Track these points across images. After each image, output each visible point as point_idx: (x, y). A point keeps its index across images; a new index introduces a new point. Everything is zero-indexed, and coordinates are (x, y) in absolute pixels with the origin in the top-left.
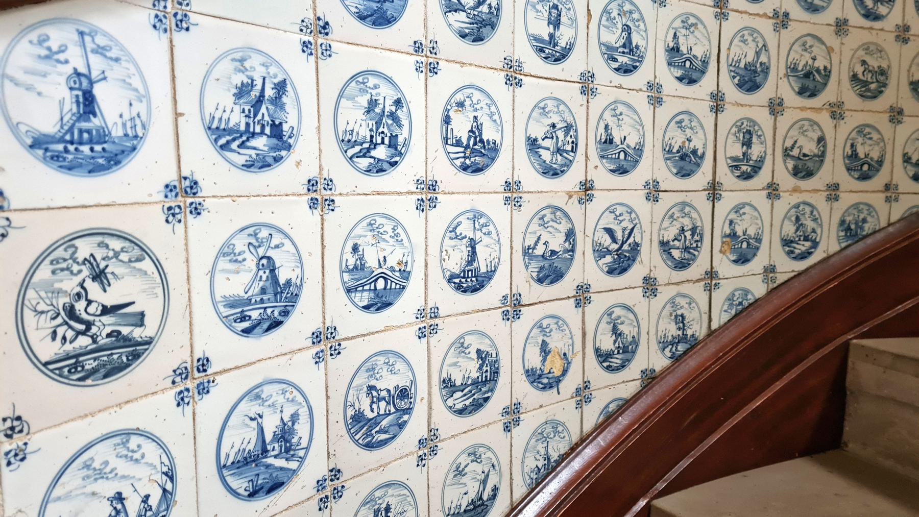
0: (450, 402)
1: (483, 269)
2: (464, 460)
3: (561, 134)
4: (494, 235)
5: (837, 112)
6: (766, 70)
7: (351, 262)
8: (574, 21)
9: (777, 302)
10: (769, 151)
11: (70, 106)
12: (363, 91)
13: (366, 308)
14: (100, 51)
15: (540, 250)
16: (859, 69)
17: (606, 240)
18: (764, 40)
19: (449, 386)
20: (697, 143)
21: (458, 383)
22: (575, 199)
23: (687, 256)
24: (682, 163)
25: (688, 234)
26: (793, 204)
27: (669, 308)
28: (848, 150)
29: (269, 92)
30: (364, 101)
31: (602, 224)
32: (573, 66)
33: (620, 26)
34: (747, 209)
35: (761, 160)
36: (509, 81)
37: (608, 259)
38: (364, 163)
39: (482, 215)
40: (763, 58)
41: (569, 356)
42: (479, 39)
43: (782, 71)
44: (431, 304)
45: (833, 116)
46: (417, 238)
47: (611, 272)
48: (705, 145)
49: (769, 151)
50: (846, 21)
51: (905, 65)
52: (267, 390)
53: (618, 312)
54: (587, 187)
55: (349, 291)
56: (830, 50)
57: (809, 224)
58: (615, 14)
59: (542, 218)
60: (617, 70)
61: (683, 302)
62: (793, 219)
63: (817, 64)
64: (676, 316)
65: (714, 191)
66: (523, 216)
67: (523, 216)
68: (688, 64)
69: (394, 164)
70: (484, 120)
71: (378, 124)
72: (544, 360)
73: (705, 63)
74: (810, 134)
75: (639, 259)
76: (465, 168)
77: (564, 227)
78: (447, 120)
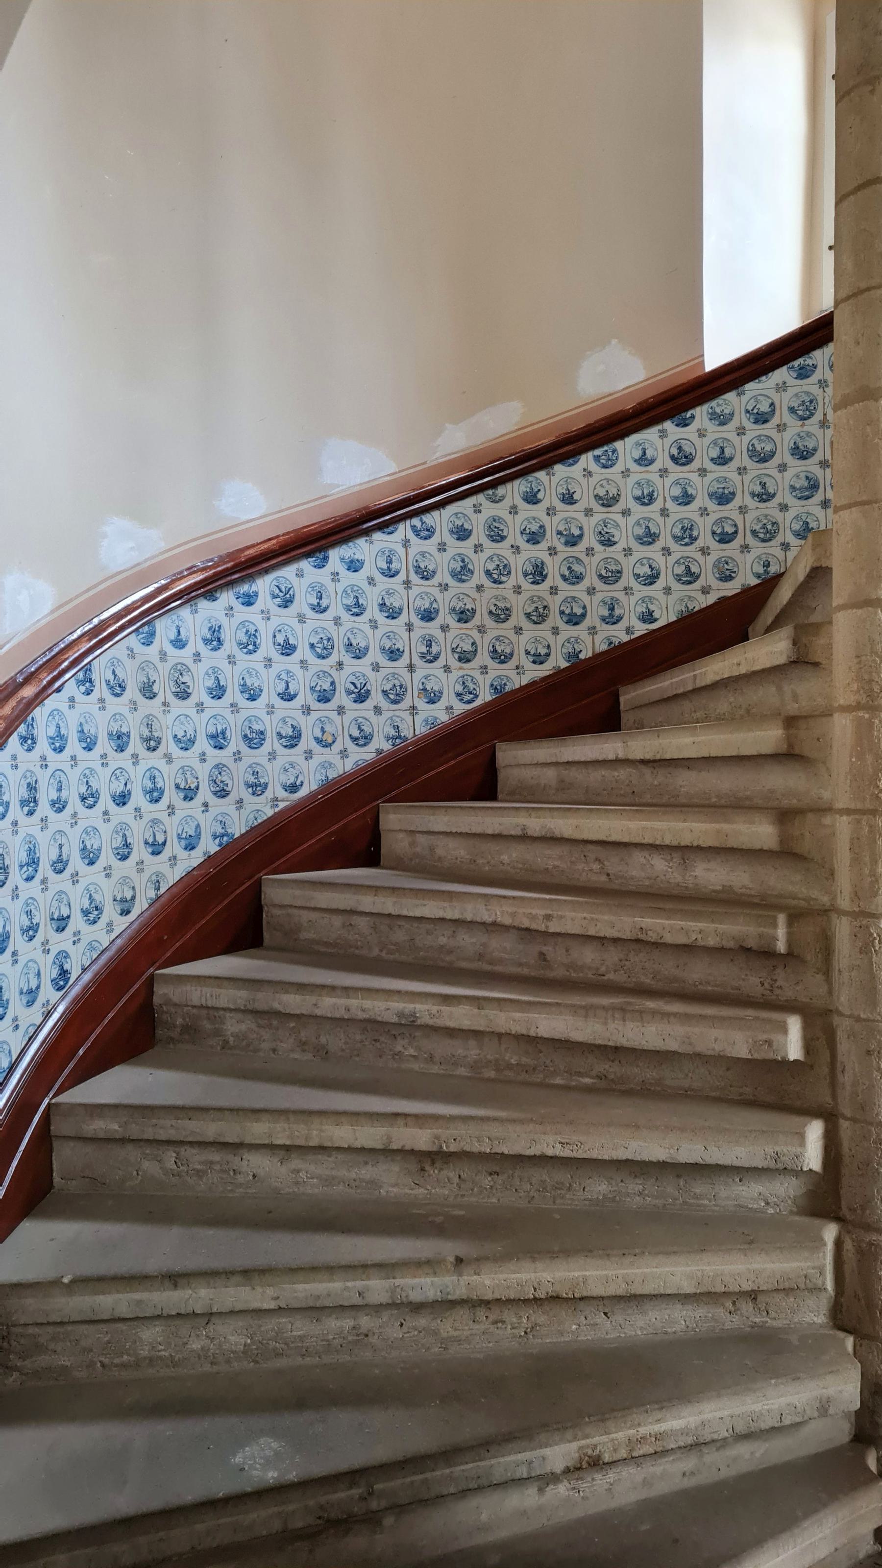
0: (280, 741)
1: (292, 693)
2: (287, 766)
3: (325, 642)
4: (296, 680)
5: (482, 630)
6: (437, 611)
7: (242, 683)
8: (329, 596)
9: (451, 724)
10: (443, 649)
11: (176, 634)
12: (244, 627)
13: (248, 699)
14: (181, 620)
15: (318, 688)
16: (493, 609)
17: (352, 688)
18: (434, 596)
19: (279, 735)
20: (399, 645)
21: (284, 735)
22: (334, 668)
23: (398, 698)
24: (391, 655)
25: (398, 688)
26: (460, 675)
28: (491, 648)
29: (217, 629)
30: (244, 630)
31: (349, 680)
32: (330, 614)
33: (352, 596)
34: (432, 677)
37: (353, 696)
38: (245, 650)
39: (290, 672)
40: (435, 605)
41: (336, 735)
42: (286, 607)
43: (447, 611)
44: (271, 703)
45: (480, 631)
46: (265, 678)
47: (355, 701)
48: (404, 647)
49: (443, 649)
50: (482, 586)
51: (521, 605)
52: (218, 717)
53: (360, 720)
54: (340, 665)
55: (241, 692)
56: (474, 600)
57: (472, 686)
58: (349, 592)
59: (318, 675)
60: (352, 615)
61: (398, 719)
62: (461, 683)
63: (467, 607)
64: (394, 726)
65: (411, 668)
68: (391, 610)
69: (255, 651)
70: (289, 636)
71: (250, 638)
72: (323, 735)
73: (401, 609)
74: (467, 641)
75: (370, 697)
76: (283, 654)
77: (330, 680)
78: (275, 636)
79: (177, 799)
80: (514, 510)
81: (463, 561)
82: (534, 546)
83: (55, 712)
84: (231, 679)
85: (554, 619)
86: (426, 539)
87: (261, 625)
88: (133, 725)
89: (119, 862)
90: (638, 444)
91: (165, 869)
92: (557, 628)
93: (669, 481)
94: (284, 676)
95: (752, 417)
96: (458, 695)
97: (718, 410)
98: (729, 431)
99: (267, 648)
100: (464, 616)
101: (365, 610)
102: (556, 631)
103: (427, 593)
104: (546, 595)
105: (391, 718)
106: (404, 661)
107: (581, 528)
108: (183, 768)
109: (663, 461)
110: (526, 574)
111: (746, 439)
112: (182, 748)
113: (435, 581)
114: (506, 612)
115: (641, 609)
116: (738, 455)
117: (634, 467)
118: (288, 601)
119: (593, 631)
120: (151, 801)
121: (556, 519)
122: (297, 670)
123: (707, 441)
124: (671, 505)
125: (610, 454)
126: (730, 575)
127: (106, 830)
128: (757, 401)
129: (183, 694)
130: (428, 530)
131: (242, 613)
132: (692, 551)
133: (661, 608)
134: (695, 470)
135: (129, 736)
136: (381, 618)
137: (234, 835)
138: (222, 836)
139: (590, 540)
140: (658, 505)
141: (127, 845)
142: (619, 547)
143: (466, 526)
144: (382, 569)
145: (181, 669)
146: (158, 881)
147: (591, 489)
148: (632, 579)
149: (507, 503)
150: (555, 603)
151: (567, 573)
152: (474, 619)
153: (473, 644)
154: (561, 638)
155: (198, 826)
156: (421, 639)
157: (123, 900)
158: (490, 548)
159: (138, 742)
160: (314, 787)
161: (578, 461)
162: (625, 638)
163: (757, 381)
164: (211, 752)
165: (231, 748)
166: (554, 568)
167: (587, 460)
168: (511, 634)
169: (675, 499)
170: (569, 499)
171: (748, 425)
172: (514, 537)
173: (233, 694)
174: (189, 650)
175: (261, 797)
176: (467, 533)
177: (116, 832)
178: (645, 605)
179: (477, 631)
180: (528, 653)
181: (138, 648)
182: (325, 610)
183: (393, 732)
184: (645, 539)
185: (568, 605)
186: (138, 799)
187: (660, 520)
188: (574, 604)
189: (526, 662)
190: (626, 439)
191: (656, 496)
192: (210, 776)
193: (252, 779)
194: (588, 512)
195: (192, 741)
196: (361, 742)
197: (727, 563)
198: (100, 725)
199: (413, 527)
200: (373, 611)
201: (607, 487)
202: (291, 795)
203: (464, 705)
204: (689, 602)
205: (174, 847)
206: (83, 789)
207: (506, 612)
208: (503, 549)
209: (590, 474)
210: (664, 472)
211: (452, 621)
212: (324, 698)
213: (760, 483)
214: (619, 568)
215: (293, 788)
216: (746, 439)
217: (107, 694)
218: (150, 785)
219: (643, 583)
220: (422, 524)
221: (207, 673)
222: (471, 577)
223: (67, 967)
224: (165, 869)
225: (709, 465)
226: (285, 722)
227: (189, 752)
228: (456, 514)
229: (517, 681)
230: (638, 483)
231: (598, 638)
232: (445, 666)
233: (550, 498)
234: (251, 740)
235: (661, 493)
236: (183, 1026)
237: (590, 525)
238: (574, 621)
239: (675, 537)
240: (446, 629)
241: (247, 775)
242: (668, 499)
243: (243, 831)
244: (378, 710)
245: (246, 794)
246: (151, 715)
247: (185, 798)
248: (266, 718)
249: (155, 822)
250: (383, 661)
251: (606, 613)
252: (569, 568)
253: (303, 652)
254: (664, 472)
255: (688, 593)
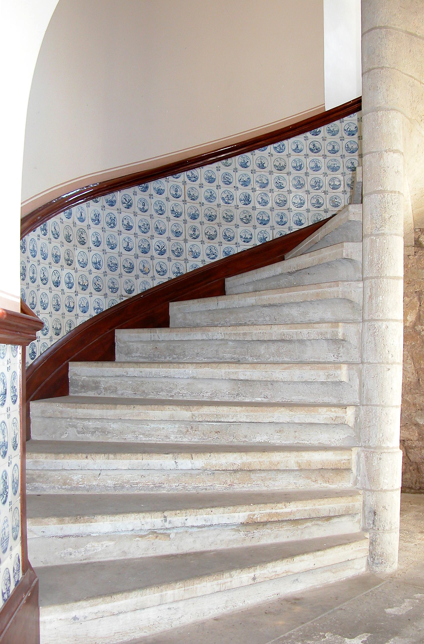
2: (127, 281)
5: (219, 225)
6: (198, 215)
8: (148, 205)
15: (142, 247)
16: (225, 215)
20: (180, 230)
24: (176, 234)
25: (179, 250)
27: (175, 265)
30: (110, 217)
35: (199, 235)
36: (134, 215)
37: (158, 251)
38: (110, 226)
41: (150, 269)
45: (218, 226)
47: (159, 254)
48: (182, 231)
49: (201, 233)
53: (161, 263)
57: (214, 251)
66: (138, 240)
67: (138, 240)
76: (126, 229)
78: (123, 221)
79: (79, 289)
80: (236, 170)
81: (211, 193)
82: (245, 187)
83: (33, 240)
84: (104, 238)
85: (254, 222)
86: (193, 181)
87: (117, 215)
88: (62, 252)
89: (55, 311)
90: (294, 143)
91: (73, 319)
92: (256, 226)
93: (309, 160)
94: (127, 240)
95: (347, 132)
96: (208, 255)
97: (331, 129)
98: (336, 138)
99: (119, 226)
100: (211, 218)
101: (164, 212)
102: (255, 227)
103: (194, 207)
104: (251, 210)
105: (176, 263)
106: (182, 237)
107: (267, 180)
108: (82, 275)
109: (306, 151)
110: (241, 200)
111: (344, 142)
112: (81, 267)
113: (198, 201)
114: (231, 217)
115: (296, 219)
116: (341, 150)
117: (293, 153)
118: (130, 206)
119: (273, 228)
120: (68, 288)
121: (255, 175)
122: (132, 237)
123: (326, 142)
124: (309, 171)
125: (281, 146)
126: (337, 204)
127: (50, 296)
128: (350, 126)
129: (83, 243)
130: (195, 178)
131: (109, 209)
132: (320, 193)
133: (305, 219)
134: (321, 155)
135: (60, 257)
136: (172, 216)
137: (103, 309)
138: (98, 309)
139: (272, 186)
140: (304, 171)
141: (58, 305)
142: (285, 189)
143: (213, 177)
144: (173, 194)
145: (81, 232)
146: (70, 324)
147: (272, 162)
148: (291, 204)
149: (232, 167)
150: (255, 214)
151: (261, 201)
152: (216, 219)
153: (215, 231)
154: (258, 230)
155: (88, 303)
156: (190, 228)
157: (56, 329)
158: (224, 187)
159: (64, 261)
160: (139, 292)
161: (266, 149)
162: (288, 232)
163: (349, 116)
164: (94, 270)
165: (103, 270)
166: (255, 197)
167: (270, 148)
168: (233, 228)
169: (312, 168)
170: (262, 166)
171: (345, 136)
172: (236, 182)
173: (104, 246)
174: (85, 224)
175: (115, 293)
176: (213, 180)
177: (54, 298)
178: (297, 217)
179: (217, 226)
180: (241, 237)
181: (65, 219)
182: (146, 211)
183: (176, 270)
184: (298, 186)
185: (261, 215)
186: (63, 285)
187: (305, 178)
188: (263, 215)
189: (240, 241)
190: (289, 140)
191: (303, 167)
192: (93, 281)
193: (111, 285)
194: (271, 173)
195: (86, 264)
196: (161, 273)
197: (336, 199)
198: (49, 250)
199: (188, 176)
200: (168, 213)
201: (280, 162)
202: (129, 294)
203: (211, 260)
204: (319, 216)
205: (77, 310)
206: (42, 276)
207: (231, 217)
208: (230, 188)
209: (272, 155)
210: (307, 156)
211: (205, 220)
212: (145, 251)
213: (351, 162)
214: (285, 199)
215: (130, 292)
216: (344, 142)
217: (52, 237)
218: (68, 280)
219: (296, 206)
220: (192, 174)
221: (93, 235)
222: (215, 200)
223: (35, 350)
224: (73, 319)
225: (328, 154)
226: (127, 261)
227: (84, 268)
228: (208, 171)
229: (236, 250)
230: (294, 160)
231: (275, 232)
232: (201, 241)
233: (253, 165)
234: (112, 267)
235: (305, 165)
236: (81, 385)
237: (272, 179)
238: (264, 223)
239: (311, 186)
240: (202, 224)
241: (109, 283)
242: (308, 168)
243: (107, 308)
244: (169, 259)
245: (108, 291)
246: (69, 249)
247: (82, 289)
248: (118, 258)
249: (69, 297)
250: (172, 236)
251: (279, 220)
252: (262, 198)
253: (136, 229)
254: (307, 156)
255: (318, 212)
